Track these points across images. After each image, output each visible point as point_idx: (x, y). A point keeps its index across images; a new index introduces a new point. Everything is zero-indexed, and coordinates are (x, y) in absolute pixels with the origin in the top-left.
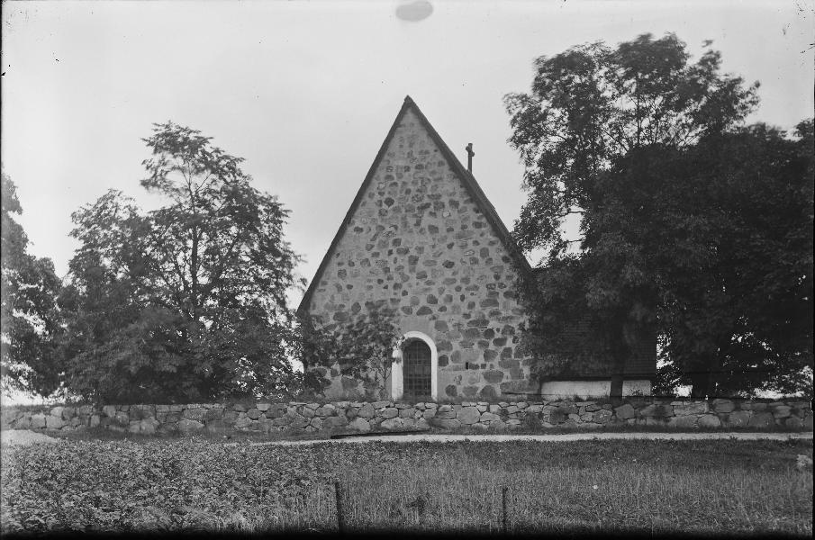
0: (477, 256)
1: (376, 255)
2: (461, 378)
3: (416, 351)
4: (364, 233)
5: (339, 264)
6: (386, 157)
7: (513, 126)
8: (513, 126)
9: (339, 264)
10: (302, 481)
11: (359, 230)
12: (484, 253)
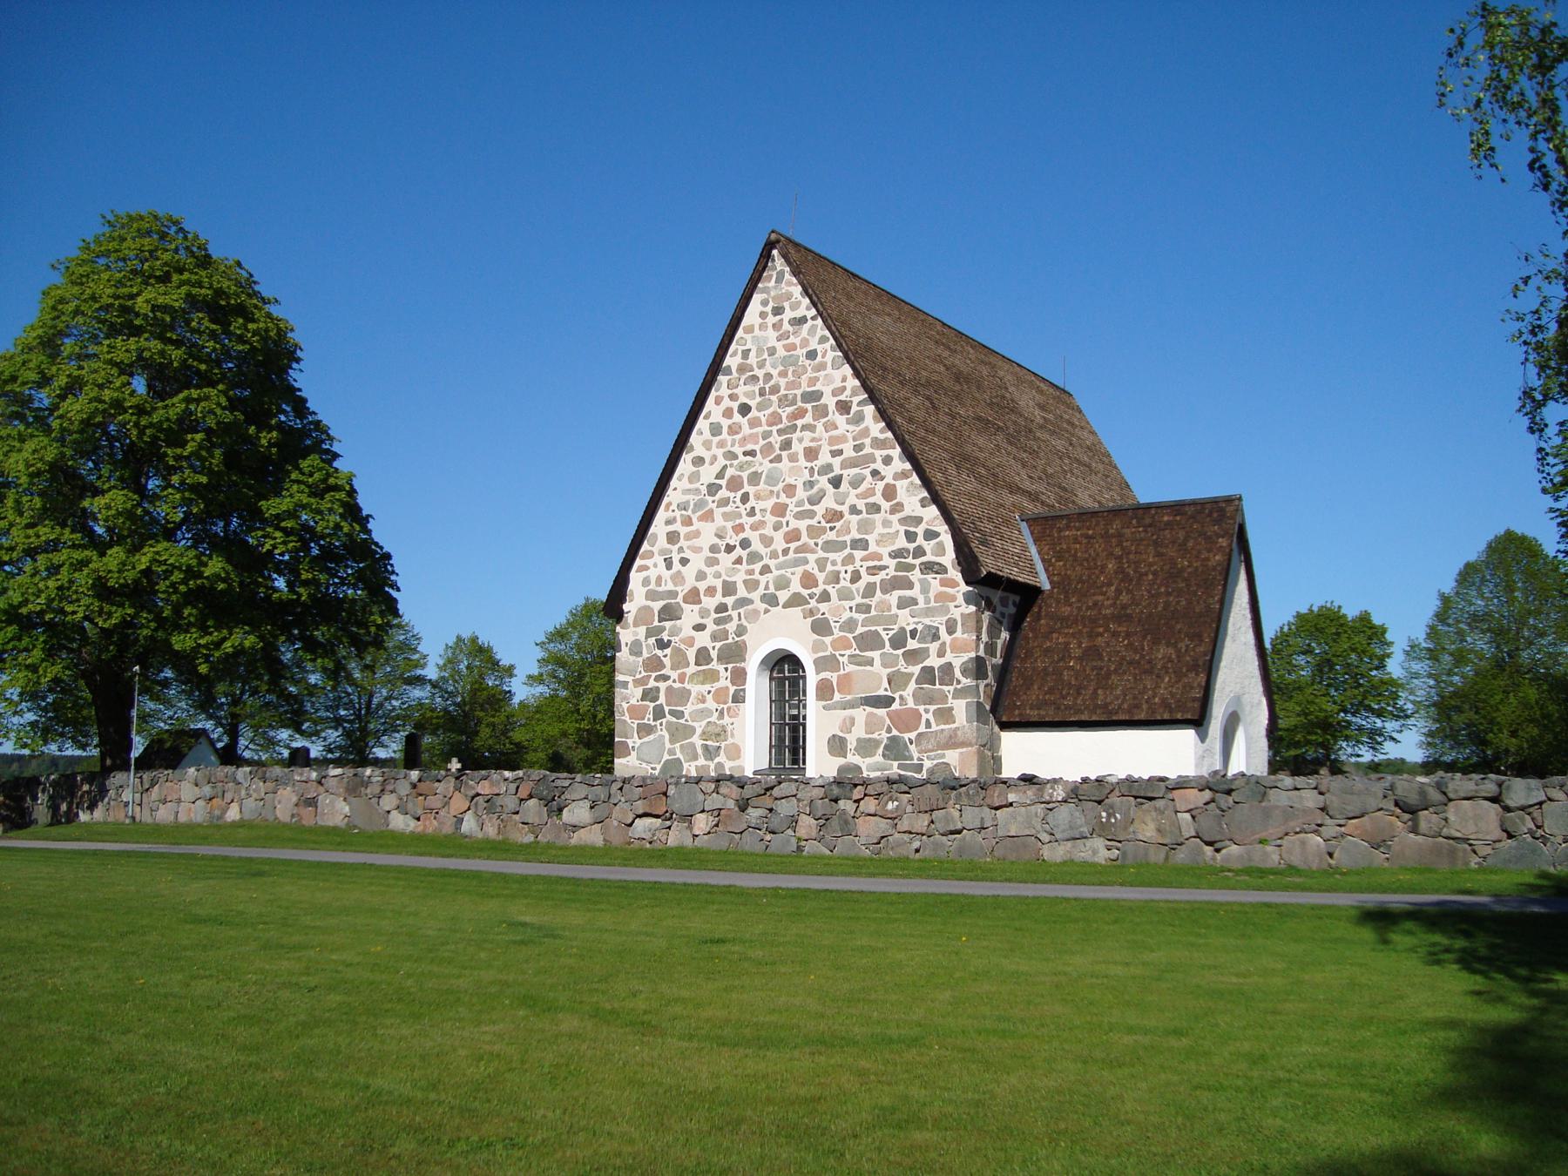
0: (878, 498)
1: (725, 502)
2: (852, 721)
3: (784, 667)
4: (706, 464)
5: (668, 522)
6: (740, 333)
7: (1392, 653)
8: (1392, 653)
9: (668, 522)
10: (823, 822)
11: (699, 461)
12: (889, 493)
